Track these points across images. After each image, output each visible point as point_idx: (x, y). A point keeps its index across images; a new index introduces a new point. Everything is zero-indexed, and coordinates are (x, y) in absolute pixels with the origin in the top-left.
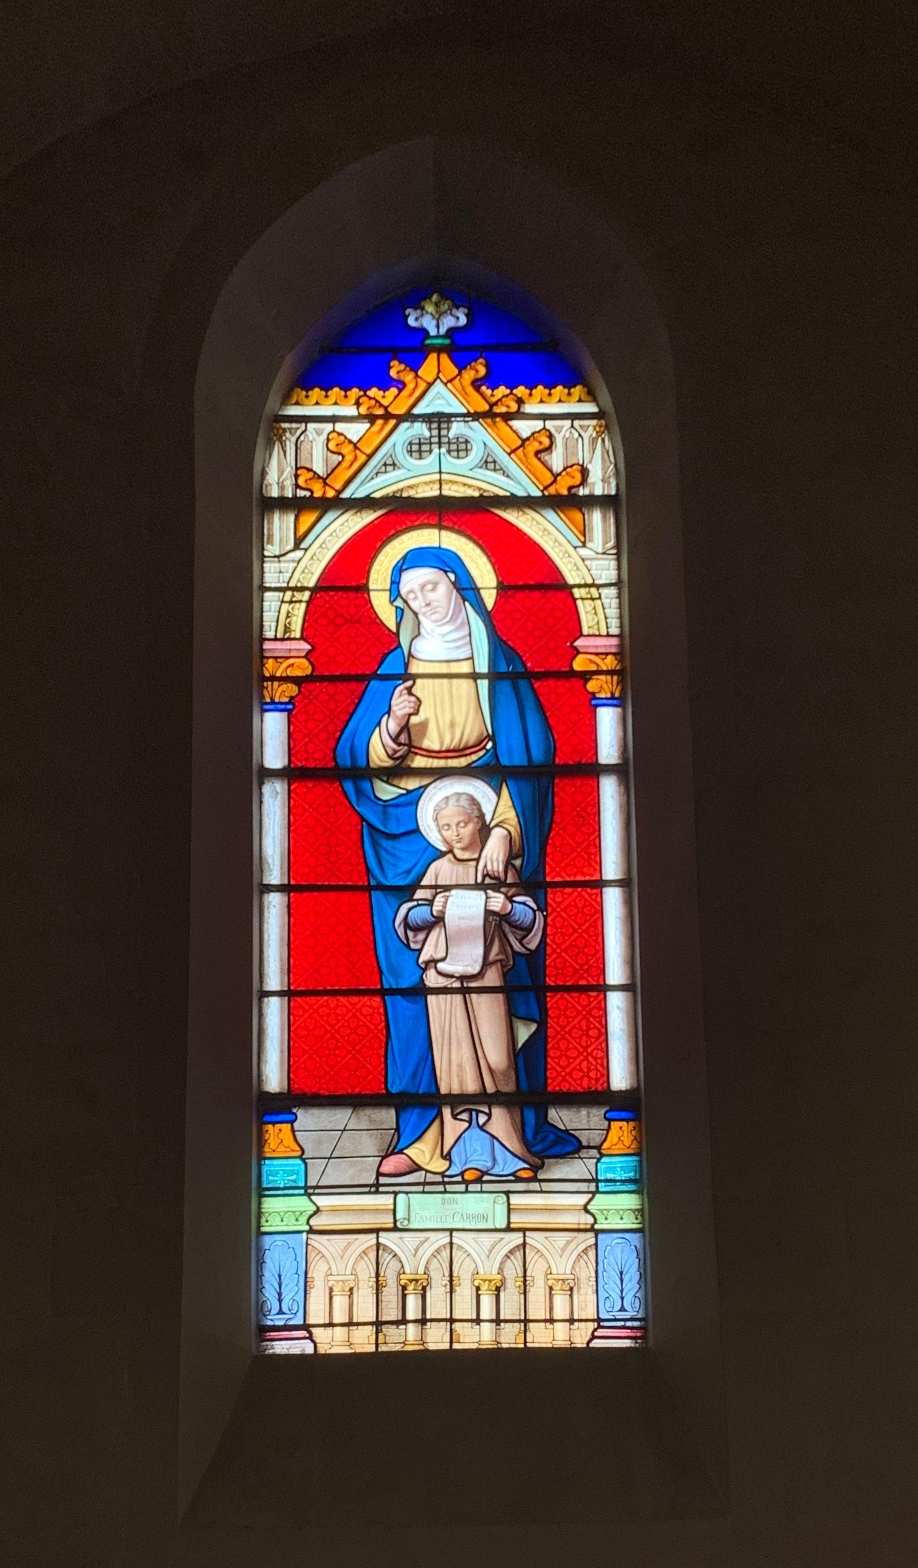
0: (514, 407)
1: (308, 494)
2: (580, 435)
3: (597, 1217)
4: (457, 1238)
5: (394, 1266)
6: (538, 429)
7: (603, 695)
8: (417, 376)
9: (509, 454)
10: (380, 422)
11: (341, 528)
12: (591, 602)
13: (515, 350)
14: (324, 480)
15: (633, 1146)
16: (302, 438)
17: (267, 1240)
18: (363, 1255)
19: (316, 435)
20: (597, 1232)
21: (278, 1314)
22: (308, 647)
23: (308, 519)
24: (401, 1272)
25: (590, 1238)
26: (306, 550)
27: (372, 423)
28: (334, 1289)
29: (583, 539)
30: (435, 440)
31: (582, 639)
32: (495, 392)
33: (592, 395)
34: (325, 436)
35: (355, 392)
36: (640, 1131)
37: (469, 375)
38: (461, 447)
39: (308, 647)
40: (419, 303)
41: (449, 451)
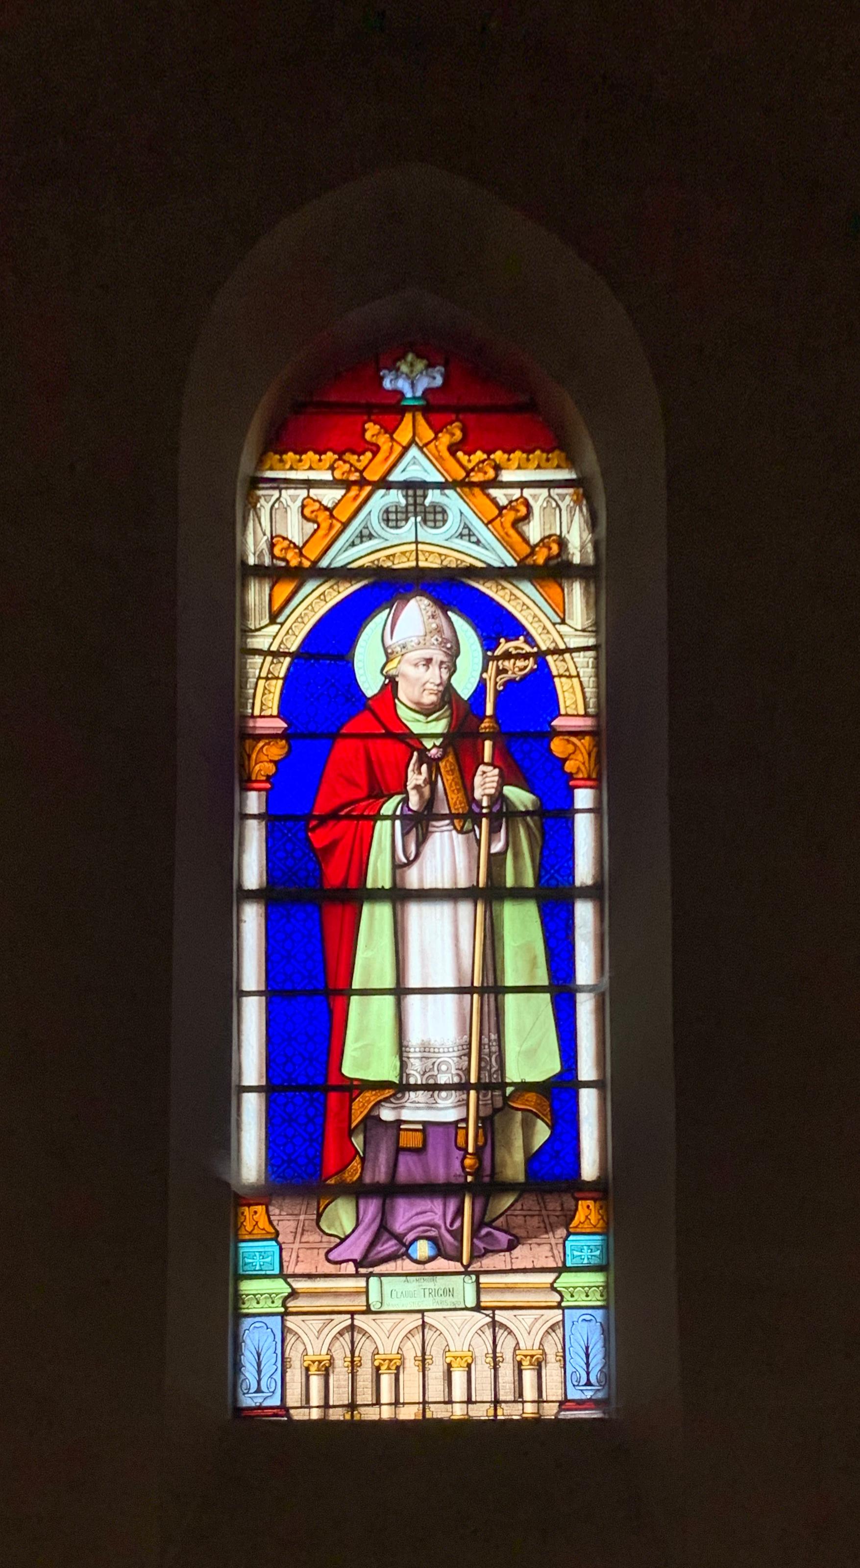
0: (491, 474)
1: (283, 564)
2: (558, 505)
3: (564, 1294)
4: (429, 1318)
5: (510, 1343)
6: (514, 498)
7: (580, 776)
8: (392, 439)
9: (486, 525)
10: (354, 491)
11: (316, 602)
12: (568, 680)
13: (494, 409)
14: (300, 549)
15: (599, 1226)
16: (276, 505)
17: (247, 1323)
18: (550, 1331)
19: (293, 498)
20: (563, 1309)
21: (256, 1392)
22: (285, 725)
23: (284, 590)
24: (305, 1352)
25: (555, 1316)
26: (282, 624)
27: (348, 490)
28: (524, 1363)
29: (562, 615)
30: (411, 508)
31: (559, 718)
32: (472, 457)
33: (571, 461)
34: (299, 503)
35: (330, 456)
36: (607, 1211)
37: (445, 439)
38: (435, 516)
39: (285, 725)
40: (394, 362)
41: (425, 521)
